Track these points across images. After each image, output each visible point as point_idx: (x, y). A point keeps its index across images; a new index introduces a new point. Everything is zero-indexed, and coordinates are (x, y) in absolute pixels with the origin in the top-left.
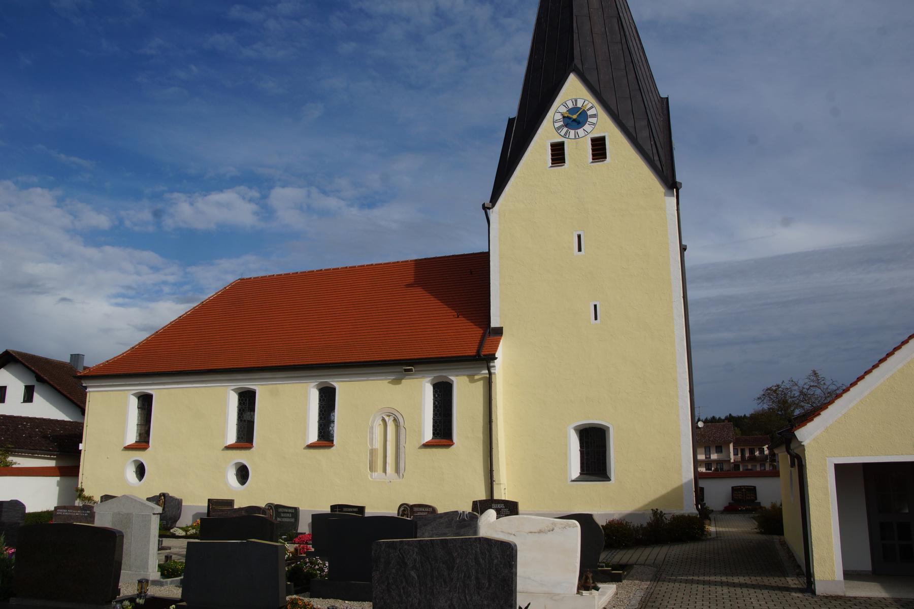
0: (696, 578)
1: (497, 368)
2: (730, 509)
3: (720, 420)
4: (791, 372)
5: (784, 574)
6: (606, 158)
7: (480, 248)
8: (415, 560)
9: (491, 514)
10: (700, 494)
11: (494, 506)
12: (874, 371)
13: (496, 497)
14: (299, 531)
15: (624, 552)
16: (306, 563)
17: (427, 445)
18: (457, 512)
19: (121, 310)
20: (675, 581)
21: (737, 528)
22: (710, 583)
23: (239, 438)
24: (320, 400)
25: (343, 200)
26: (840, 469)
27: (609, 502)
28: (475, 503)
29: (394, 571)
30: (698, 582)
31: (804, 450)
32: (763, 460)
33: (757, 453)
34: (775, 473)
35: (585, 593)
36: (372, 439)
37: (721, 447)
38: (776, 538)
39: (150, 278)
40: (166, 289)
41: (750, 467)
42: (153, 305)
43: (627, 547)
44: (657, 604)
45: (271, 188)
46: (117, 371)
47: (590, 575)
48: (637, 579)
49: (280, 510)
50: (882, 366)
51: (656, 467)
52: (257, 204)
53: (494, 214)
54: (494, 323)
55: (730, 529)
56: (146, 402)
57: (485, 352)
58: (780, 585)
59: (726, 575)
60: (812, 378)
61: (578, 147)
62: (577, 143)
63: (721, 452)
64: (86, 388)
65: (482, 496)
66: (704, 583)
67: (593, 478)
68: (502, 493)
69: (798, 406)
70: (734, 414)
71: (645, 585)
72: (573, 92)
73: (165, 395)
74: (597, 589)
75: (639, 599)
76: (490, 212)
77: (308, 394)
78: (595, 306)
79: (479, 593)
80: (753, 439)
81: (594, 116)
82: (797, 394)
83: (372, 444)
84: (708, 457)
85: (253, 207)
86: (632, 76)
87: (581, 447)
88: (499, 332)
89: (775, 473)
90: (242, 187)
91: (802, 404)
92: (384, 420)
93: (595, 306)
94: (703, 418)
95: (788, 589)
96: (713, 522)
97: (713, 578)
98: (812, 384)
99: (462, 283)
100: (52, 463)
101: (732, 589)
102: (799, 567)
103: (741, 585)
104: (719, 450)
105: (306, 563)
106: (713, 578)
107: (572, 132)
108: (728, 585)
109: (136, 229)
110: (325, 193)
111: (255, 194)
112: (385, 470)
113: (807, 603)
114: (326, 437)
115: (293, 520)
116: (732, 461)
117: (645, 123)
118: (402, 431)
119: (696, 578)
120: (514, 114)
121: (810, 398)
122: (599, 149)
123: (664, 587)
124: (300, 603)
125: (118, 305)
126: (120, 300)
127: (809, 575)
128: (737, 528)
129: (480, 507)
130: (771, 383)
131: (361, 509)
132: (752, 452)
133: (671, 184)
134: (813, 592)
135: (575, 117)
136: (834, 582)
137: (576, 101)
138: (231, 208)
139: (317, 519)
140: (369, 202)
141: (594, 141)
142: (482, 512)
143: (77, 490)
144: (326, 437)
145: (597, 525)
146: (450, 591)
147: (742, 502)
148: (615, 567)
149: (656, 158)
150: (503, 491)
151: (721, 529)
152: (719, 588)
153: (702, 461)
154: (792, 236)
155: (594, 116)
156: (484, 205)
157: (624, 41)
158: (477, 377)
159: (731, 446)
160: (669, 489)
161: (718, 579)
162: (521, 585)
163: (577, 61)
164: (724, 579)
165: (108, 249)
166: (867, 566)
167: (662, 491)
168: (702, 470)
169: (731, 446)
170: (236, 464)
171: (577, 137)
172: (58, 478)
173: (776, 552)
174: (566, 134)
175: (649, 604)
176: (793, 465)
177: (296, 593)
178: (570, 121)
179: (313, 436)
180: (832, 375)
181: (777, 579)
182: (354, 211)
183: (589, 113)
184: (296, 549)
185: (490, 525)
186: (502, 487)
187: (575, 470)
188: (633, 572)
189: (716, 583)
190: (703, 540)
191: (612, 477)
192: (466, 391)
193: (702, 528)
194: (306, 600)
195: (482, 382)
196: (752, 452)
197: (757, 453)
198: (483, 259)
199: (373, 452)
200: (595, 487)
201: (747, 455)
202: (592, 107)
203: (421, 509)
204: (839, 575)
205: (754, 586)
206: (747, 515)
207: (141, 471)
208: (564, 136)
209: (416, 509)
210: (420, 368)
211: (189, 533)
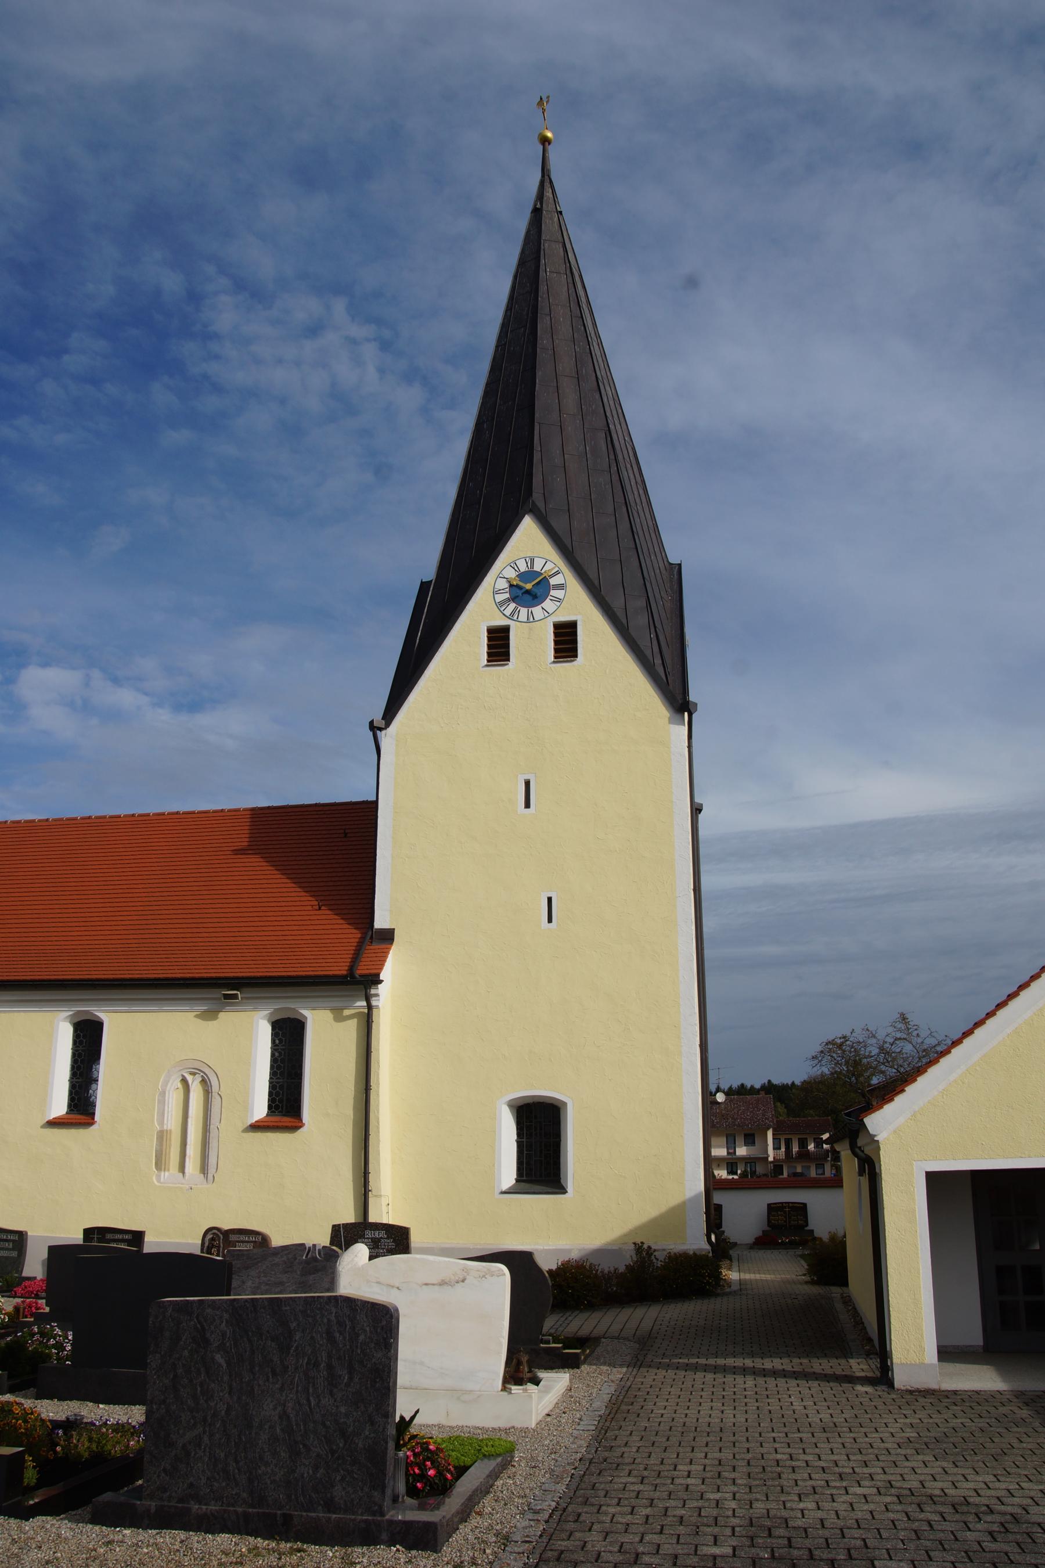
0: (702, 1361)
1: (382, 998)
2: (765, 1242)
3: (752, 1091)
4: (864, 1015)
5: (845, 1353)
6: (576, 656)
7: (365, 795)
8: (224, 1334)
9: (360, 1251)
10: (714, 1216)
11: (369, 1234)
12: (989, 1022)
13: (372, 1218)
14: (24, 1274)
15: (586, 1315)
16: (33, 1335)
17: (257, 1127)
18: (303, 1245)
20: (668, 1367)
21: (772, 1274)
22: (725, 1370)
24: (75, 1043)
25: (146, 694)
26: (936, 1182)
27: (560, 1230)
28: (336, 1229)
29: (186, 1353)
30: (706, 1368)
31: (879, 1148)
32: (819, 1159)
33: (811, 1147)
34: (836, 1183)
35: (515, 1389)
36: (162, 1114)
37: (753, 1135)
38: (836, 1291)
41: (799, 1170)
43: (591, 1307)
44: (636, 1407)
47: (525, 1359)
48: (604, 1364)
50: (1001, 1013)
51: (643, 1170)
53: (387, 738)
54: (381, 922)
55: (763, 1277)
57: (361, 970)
58: (839, 1372)
59: (752, 1355)
60: (900, 1025)
61: (531, 637)
62: (530, 629)
63: (753, 1143)
65: (348, 1216)
66: (715, 1369)
68: (383, 1212)
69: (876, 1071)
70: (775, 1082)
71: (618, 1373)
72: (528, 545)
74: (536, 1382)
75: (607, 1398)
76: (381, 735)
78: (550, 900)
79: (332, 1394)
80: (800, 1124)
81: (560, 587)
82: (875, 1051)
83: (161, 1122)
84: (732, 1153)
86: (624, 526)
87: (519, 1134)
88: (387, 936)
89: (836, 1183)
91: (883, 1068)
92: (184, 1081)
93: (550, 900)
94: (725, 1086)
95: (851, 1379)
96: (735, 1264)
97: (730, 1361)
98: (899, 1035)
99: (329, 852)
101: (761, 1380)
102: (870, 1340)
103: (775, 1373)
104: (749, 1140)
105: (33, 1335)
106: (730, 1361)
107: (524, 611)
108: (755, 1372)
110: (116, 681)
112: (182, 1168)
113: (878, 1402)
114: (82, 1105)
115: (14, 1254)
116: (771, 1159)
117: (642, 603)
118: (216, 1101)
119: (702, 1361)
120: (430, 573)
121: (894, 1059)
123: (651, 1377)
124: (17, 1410)
127: (882, 1352)
128: (772, 1274)
129: (345, 1236)
130: (834, 1031)
131: (137, 1237)
132: (803, 1144)
133: (680, 703)
134: (890, 1384)
135: (529, 586)
136: (922, 1366)
137: (532, 561)
139: (58, 1254)
140: (191, 701)
142: (348, 1245)
144: (82, 1105)
145: (539, 1270)
146: (282, 1389)
147: (785, 1229)
148: (569, 1343)
149: (658, 661)
150: (384, 1209)
151: (747, 1276)
152: (740, 1379)
153: (719, 1161)
154: (873, 788)
155: (560, 587)
156: (371, 723)
157: (614, 468)
158: (347, 1012)
159: (770, 1134)
161: (739, 1362)
162: (405, 1375)
163: (537, 496)
164: (749, 1362)
166: (975, 1337)
168: (722, 1173)
169: (770, 1134)
170: (670, 722)
171: (531, 619)
173: (831, 1318)
174: (512, 614)
175: (624, 1407)
176: (861, 1173)
177: (12, 1390)
178: (520, 593)
179: (59, 1106)
180: (931, 1023)
181: (834, 1362)
182: (164, 716)
183: (553, 581)
184: (17, 1309)
185: (359, 1274)
186: (384, 1201)
187: (508, 1175)
188: (599, 1350)
189: (734, 1370)
190: (717, 1295)
191: (570, 1187)
192: (327, 1035)
193: (717, 1276)
194: (28, 1403)
195: (355, 1020)
196: (803, 1144)
197: (811, 1147)
198: (365, 815)
199: (162, 1136)
201: (795, 1149)
202: (557, 573)
204: (931, 1354)
205: (796, 1375)
206: (791, 1252)
208: (510, 617)
210: (249, 993)
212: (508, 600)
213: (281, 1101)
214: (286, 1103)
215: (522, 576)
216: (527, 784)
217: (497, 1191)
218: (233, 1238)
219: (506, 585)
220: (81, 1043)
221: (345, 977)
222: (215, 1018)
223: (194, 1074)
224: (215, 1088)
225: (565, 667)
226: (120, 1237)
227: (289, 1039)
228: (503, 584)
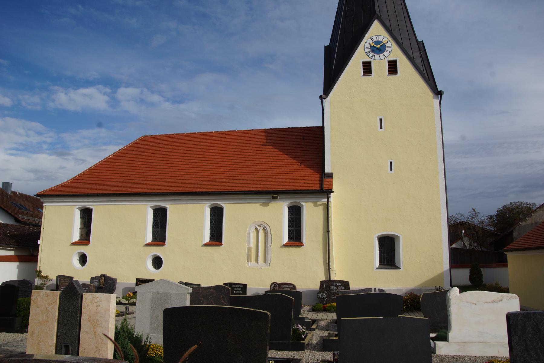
13: (331, 279)
17: (206, 245)
19: (13, 157)
23: (290, 238)
24: (211, 215)
25: (162, 96)
29: (530, 335)
36: (248, 241)
39: (35, 139)
40: (45, 146)
42: (35, 156)
45: (118, 87)
46: (62, 193)
49: (234, 286)
52: (108, 96)
53: (327, 102)
54: (327, 170)
56: (87, 214)
61: (380, 65)
62: (379, 63)
64: (43, 203)
67: (389, 267)
72: (376, 31)
73: (101, 210)
76: (324, 100)
77: (202, 211)
78: (391, 163)
83: (248, 244)
85: (106, 98)
88: (331, 175)
90: (100, 86)
92: (256, 229)
93: (391, 163)
99: (308, 145)
100: (11, 253)
107: (376, 56)
109: (29, 107)
110: (153, 93)
111: (108, 90)
112: (257, 261)
117: (418, 54)
118: (269, 236)
122: (393, 67)
125: (12, 155)
126: (14, 152)
135: (378, 46)
138: (94, 98)
140: (178, 100)
141: (390, 62)
143: (37, 271)
158: (319, 203)
160: (436, 275)
165: (8, 119)
167: (431, 276)
171: (379, 59)
172: (18, 263)
174: (372, 57)
182: (167, 105)
183: (387, 45)
192: (311, 212)
199: (249, 249)
200: (389, 273)
203: (286, 286)
207: (83, 259)
208: (371, 58)
209: (282, 286)
211: (130, 302)
212: (370, 51)
213: (293, 236)
214: (295, 236)
215: (375, 42)
216: (381, 120)
217: (375, 268)
218: (282, 286)
219: (369, 46)
220: (214, 215)
221: (320, 190)
222: (268, 206)
223: (260, 226)
224: (269, 231)
225: (393, 77)
226: (238, 286)
227: (295, 215)
228: (368, 45)
